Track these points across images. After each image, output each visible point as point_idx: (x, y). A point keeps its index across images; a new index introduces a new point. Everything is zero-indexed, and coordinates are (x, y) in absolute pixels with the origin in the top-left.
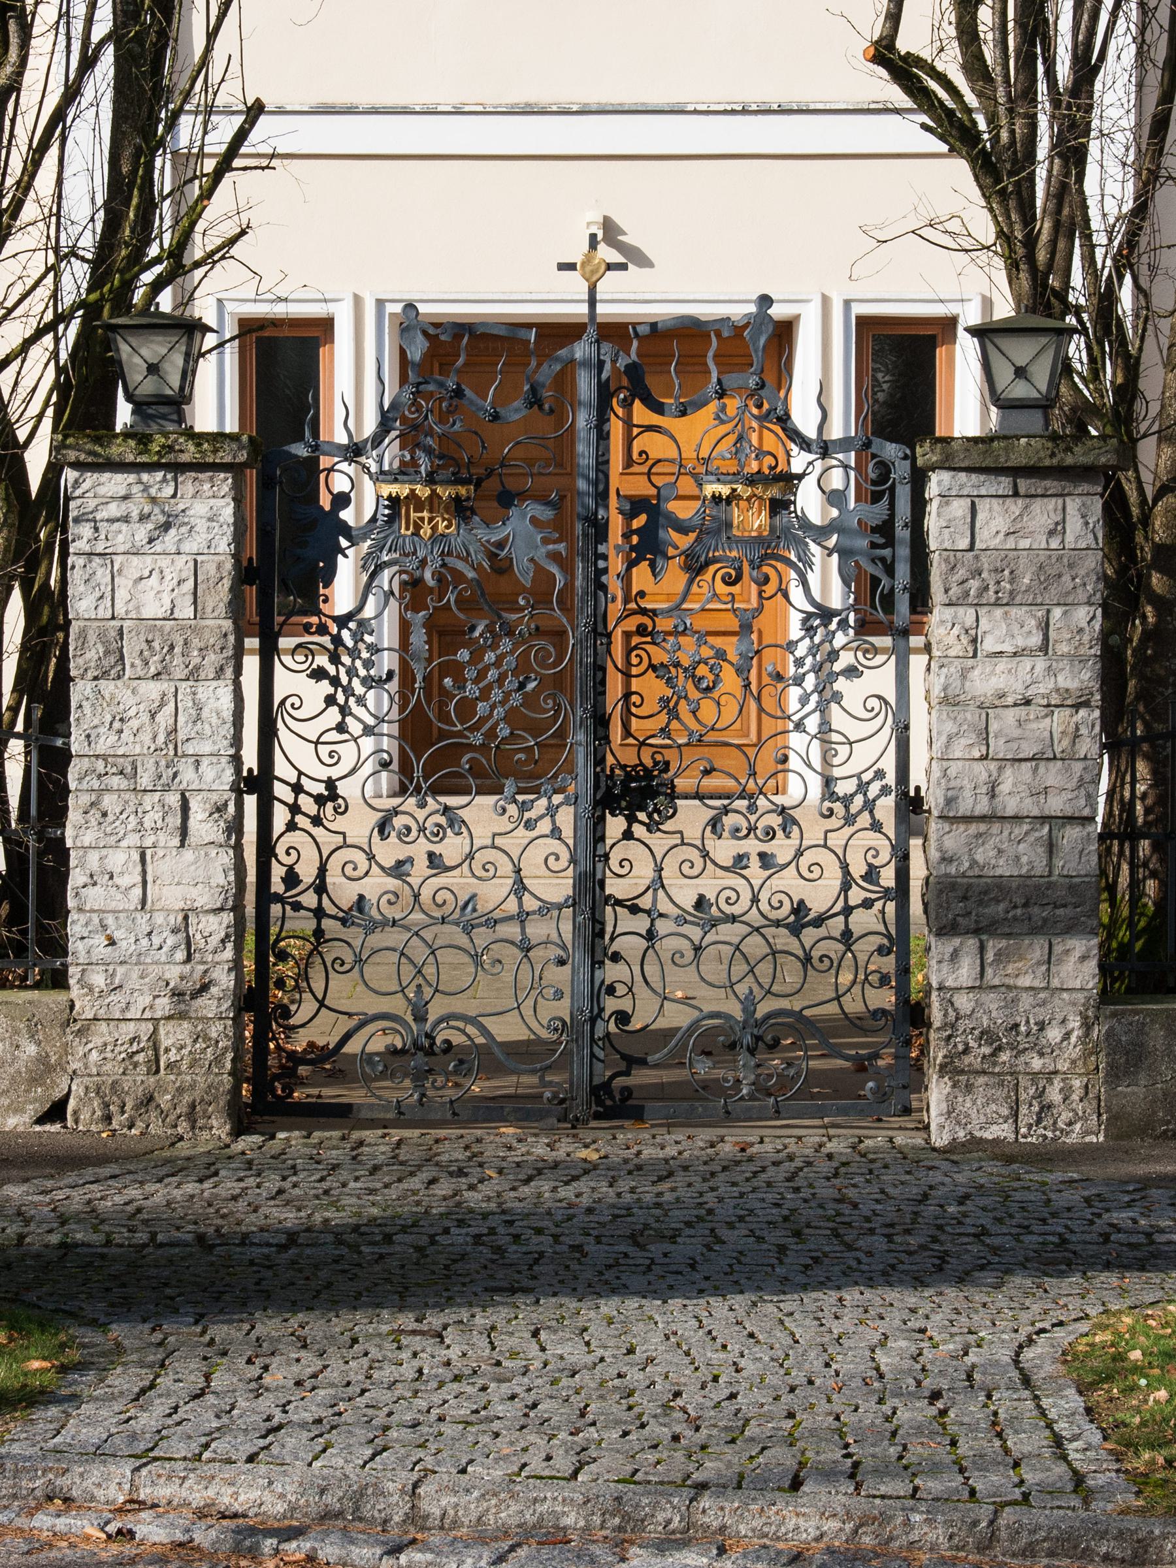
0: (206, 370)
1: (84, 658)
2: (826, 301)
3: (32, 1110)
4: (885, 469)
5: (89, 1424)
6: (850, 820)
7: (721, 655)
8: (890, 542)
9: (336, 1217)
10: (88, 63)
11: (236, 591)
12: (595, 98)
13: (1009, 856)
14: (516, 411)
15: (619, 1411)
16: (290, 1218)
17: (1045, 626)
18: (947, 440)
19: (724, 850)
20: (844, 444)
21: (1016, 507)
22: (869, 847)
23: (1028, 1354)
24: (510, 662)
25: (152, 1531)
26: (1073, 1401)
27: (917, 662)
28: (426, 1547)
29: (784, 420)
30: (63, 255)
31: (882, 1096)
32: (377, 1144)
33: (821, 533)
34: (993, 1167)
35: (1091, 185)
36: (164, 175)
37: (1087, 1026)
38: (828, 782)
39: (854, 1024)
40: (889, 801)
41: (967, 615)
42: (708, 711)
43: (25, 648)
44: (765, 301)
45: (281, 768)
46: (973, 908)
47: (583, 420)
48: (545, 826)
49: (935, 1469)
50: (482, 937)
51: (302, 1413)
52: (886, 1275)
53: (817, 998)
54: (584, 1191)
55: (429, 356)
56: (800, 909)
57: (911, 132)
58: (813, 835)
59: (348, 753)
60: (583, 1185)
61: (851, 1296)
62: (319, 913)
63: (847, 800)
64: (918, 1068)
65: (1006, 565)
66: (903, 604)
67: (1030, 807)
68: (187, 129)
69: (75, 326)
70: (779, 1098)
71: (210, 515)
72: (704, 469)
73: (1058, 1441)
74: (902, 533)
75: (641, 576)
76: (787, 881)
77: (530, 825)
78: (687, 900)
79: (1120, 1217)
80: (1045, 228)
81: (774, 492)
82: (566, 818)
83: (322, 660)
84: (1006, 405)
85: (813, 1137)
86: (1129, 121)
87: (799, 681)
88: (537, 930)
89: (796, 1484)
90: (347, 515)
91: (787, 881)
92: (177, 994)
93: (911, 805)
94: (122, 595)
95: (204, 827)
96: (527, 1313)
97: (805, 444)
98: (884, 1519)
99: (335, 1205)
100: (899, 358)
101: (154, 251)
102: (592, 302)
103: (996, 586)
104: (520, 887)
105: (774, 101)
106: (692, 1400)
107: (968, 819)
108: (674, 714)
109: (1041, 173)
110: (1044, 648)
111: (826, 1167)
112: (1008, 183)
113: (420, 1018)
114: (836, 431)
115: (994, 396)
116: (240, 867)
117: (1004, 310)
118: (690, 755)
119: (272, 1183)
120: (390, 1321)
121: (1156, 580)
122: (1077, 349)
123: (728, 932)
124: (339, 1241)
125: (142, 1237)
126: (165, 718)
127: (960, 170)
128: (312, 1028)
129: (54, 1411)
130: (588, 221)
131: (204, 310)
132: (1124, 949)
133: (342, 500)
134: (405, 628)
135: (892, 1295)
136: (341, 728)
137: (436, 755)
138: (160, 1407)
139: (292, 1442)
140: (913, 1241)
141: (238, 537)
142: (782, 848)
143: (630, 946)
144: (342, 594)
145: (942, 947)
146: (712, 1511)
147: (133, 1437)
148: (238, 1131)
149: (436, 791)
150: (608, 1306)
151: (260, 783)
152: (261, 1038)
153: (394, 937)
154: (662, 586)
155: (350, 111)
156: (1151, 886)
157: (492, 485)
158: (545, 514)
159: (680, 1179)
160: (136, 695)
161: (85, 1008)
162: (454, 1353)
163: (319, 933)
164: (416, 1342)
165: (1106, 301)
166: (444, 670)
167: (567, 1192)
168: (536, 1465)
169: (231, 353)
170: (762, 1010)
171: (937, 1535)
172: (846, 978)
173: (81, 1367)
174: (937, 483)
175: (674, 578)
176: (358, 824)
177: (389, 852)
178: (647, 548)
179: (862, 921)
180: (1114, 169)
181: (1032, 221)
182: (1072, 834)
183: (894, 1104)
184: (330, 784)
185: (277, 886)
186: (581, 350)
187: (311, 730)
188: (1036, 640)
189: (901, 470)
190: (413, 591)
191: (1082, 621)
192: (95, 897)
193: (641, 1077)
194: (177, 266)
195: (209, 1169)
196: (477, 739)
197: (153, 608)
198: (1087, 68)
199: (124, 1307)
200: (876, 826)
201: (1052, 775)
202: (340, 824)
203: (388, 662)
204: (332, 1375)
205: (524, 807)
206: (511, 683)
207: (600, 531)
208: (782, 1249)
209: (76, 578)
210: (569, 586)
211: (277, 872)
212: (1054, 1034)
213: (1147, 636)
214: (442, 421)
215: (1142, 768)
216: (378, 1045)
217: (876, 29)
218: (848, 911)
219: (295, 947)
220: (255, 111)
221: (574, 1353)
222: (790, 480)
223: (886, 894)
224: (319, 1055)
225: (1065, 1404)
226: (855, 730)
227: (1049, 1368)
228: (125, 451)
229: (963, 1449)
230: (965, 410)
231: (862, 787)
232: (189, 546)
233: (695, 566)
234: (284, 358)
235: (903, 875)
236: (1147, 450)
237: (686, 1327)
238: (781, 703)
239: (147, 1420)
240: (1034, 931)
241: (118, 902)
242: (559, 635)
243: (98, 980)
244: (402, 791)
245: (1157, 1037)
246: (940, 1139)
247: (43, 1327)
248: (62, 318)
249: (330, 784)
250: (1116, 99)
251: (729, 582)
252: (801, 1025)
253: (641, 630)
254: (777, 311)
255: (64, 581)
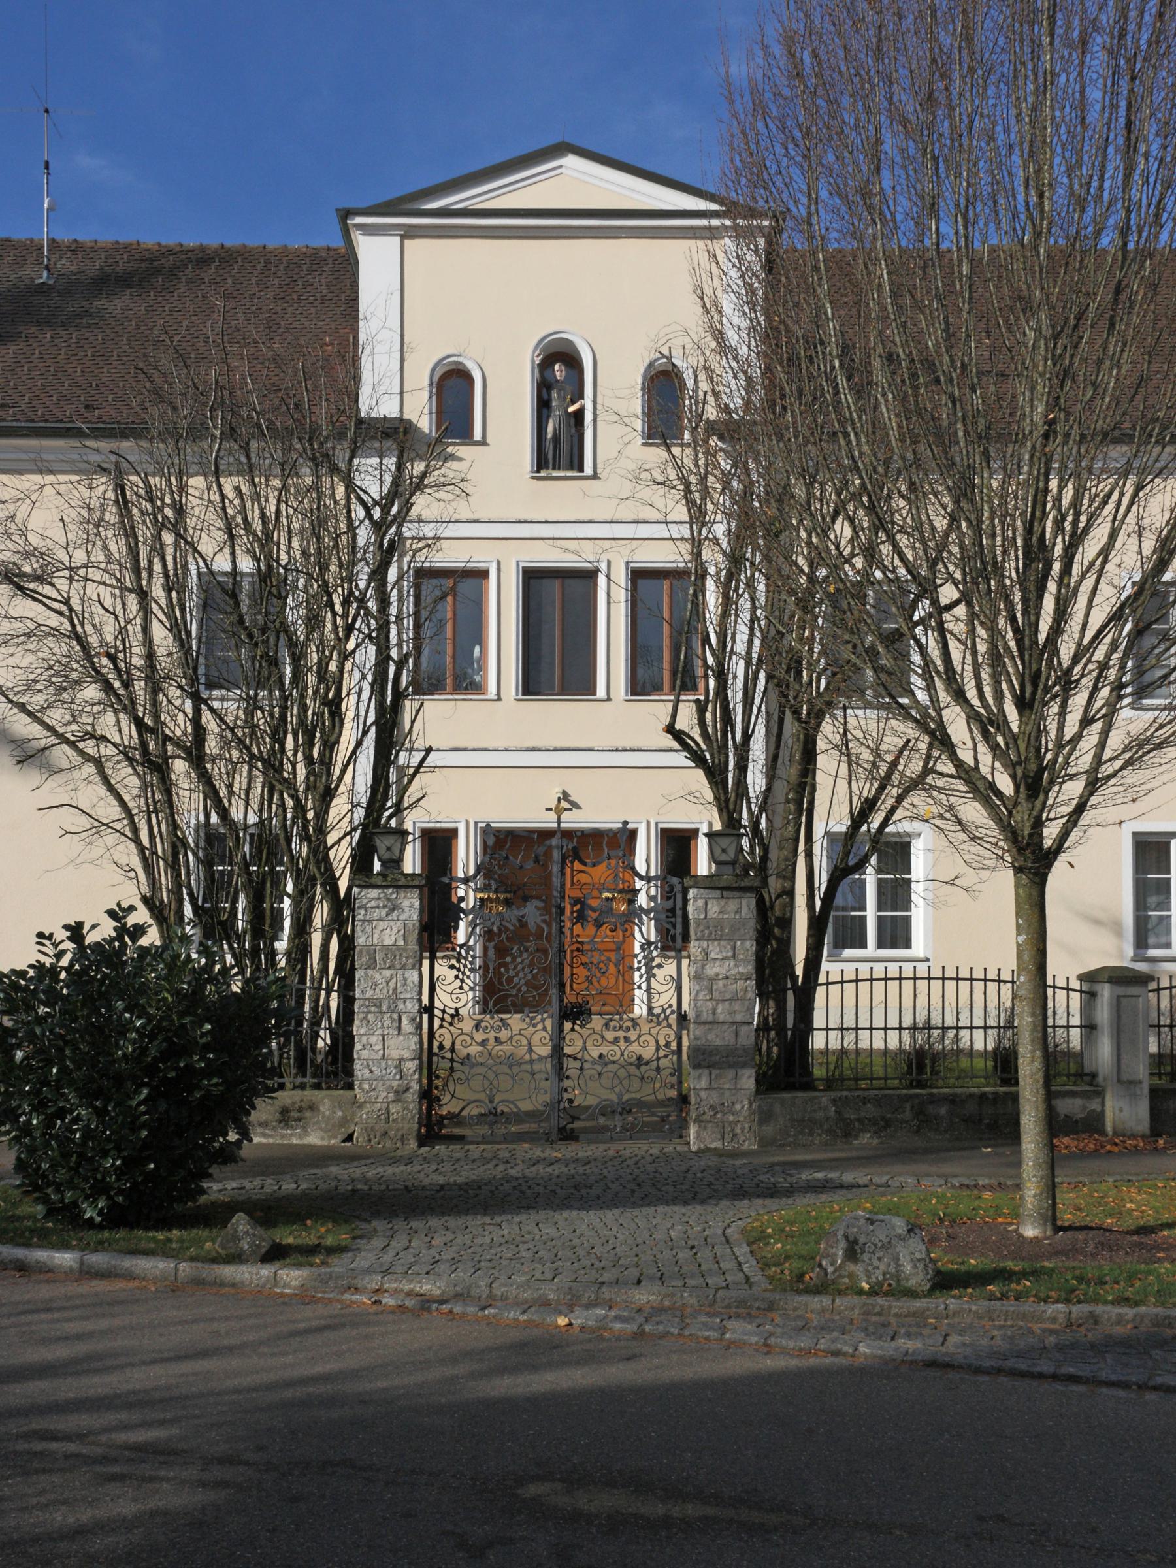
0: (409, 849)
1: (361, 960)
2: (648, 823)
3: (340, 1137)
4: (672, 888)
5: (364, 1260)
6: (659, 1024)
7: (609, 959)
8: (674, 916)
9: (459, 1180)
10: (365, 732)
11: (420, 934)
12: (559, 745)
13: (719, 1038)
14: (530, 865)
15: (569, 1254)
16: (441, 1180)
17: (734, 948)
18: (696, 876)
19: (610, 1036)
20: (656, 878)
21: (722, 902)
22: (666, 1034)
23: (728, 1231)
24: (527, 962)
25: (389, 1301)
26: (745, 1249)
27: (685, 962)
28: (495, 1307)
29: (633, 868)
30: (355, 805)
31: (671, 1131)
32: (475, 1150)
33: (647, 912)
34: (715, 1159)
35: (749, 780)
36: (393, 775)
37: (751, 1104)
38: (650, 1009)
39: (661, 1103)
40: (674, 1016)
41: (705, 944)
42: (604, 981)
43: (338, 957)
44: (625, 823)
45: (437, 1004)
46: (704, 1058)
47: (555, 869)
48: (540, 1026)
49: (692, 1276)
50: (515, 1070)
51: (447, 1256)
52: (674, 1201)
53: (646, 1093)
54: (556, 1170)
55: (496, 843)
56: (640, 1058)
57: (681, 759)
58: (645, 1030)
59: (463, 997)
60: (555, 1166)
61: (660, 1209)
62: (452, 1060)
63: (658, 1016)
64: (685, 1120)
65: (719, 923)
66: (679, 939)
67: (729, 1019)
68: (403, 758)
69: (358, 833)
70: (632, 1132)
71: (411, 905)
72: (602, 887)
73: (740, 1264)
74: (679, 913)
75: (578, 929)
76: (635, 1047)
77: (535, 1026)
78: (595, 1054)
79: (762, 1178)
80: (732, 796)
81: (629, 896)
82: (549, 1023)
83: (454, 962)
84: (718, 863)
85: (645, 1147)
86: (763, 756)
87: (639, 969)
88: (536, 1067)
89: (639, 1282)
90: (463, 905)
91: (635, 1047)
92: (397, 1092)
93: (682, 1018)
94: (376, 936)
95: (406, 1026)
96: (534, 1216)
97: (641, 878)
98: (672, 1295)
99: (458, 1174)
100: (677, 844)
101: (389, 804)
102: (559, 822)
103: (715, 931)
104: (530, 1050)
105: (628, 745)
106: (598, 1250)
107: (705, 1023)
108: (590, 982)
109: (731, 775)
110: (734, 956)
111: (649, 1159)
112: (718, 778)
113: (491, 1101)
114: (653, 874)
115: (713, 857)
116: (421, 1042)
117: (718, 826)
118: (597, 998)
119: (434, 1167)
120: (480, 1220)
121: (776, 931)
122: (745, 843)
123: (610, 1067)
124: (460, 1189)
125: (383, 1187)
126: (392, 984)
127: (700, 773)
128: (448, 1105)
129: (350, 1254)
130: (556, 793)
131: (408, 826)
132: (765, 1073)
133: (462, 899)
134: (485, 949)
135: (676, 1208)
136: (461, 988)
137: (496, 997)
138: (391, 1253)
139: (442, 1267)
140: (684, 1187)
141: (421, 913)
142: (633, 1034)
143: (574, 1073)
144: (461, 936)
145: (694, 1073)
146: (606, 1293)
147: (382, 1264)
148: (421, 1145)
149: (498, 1012)
150: (566, 1214)
151: (429, 1009)
152: (429, 1109)
153: (482, 1070)
154: (585, 932)
155: (465, 750)
156: (775, 1049)
157: (520, 893)
158: (542, 904)
159: (593, 1164)
160: (381, 976)
161: (361, 1097)
162: (505, 1232)
163: (452, 1068)
164: (491, 1228)
165: (755, 824)
166: (500, 965)
167: (549, 1170)
168: (538, 1275)
169: (418, 843)
170: (625, 1098)
171: (693, 1301)
172: (657, 1085)
173: (361, 1237)
174: (692, 893)
175: (591, 929)
176: (467, 1026)
177: (479, 1037)
178: (581, 917)
179: (664, 1063)
180: (759, 774)
181: (728, 799)
182: (744, 1030)
183: (676, 1134)
184: (457, 1010)
185: (436, 1050)
186: (555, 842)
187: (449, 989)
188: (730, 954)
189: (678, 888)
190: (488, 935)
191: (750, 946)
192: (365, 1054)
193: (577, 1124)
194: (398, 809)
195: (409, 1161)
196: (514, 992)
197: (388, 941)
198: (747, 737)
199: (376, 1214)
200: (669, 1026)
201: (737, 1006)
202: (460, 1025)
203: (478, 962)
204: (459, 1241)
205: (532, 1019)
206: (527, 970)
207: (562, 911)
208: (633, 1191)
209: (358, 929)
210: (550, 933)
211: (436, 1044)
212: (738, 1107)
213: (773, 952)
214: (500, 867)
215: (771, 1003)
216: (475, 1112)
217: (667, 720)
218: (658, 1059)
219: (442, 1073)
220: (429, 750)
221: (552, 1232)
222: (635, 892)
223: (673, 1052)
224: (452, 1116)
225: (742, 1250)
226: (661, 988)
227: (737, 1236)
228: (374, 880)
229: (703, 1267)
230: (703, 865)
231: (664, 1011)
232: (403, 917)
233: (599, 925)
234: (438, 843)
235: (679, 1045)
236: (772, 881)
237: (596, 1222)
238: (632, 978)
239: (387, 1258)
240: (730, 1066)
241: (374, 1056)
242: (545, 952)
243: (366, 1086)
244: (484, 1012)
245: (777, 1108)
246: (694, 1148)
247: (346, 1221)
248: (354, 829)
249: (457, 1010)
250: (758, 747)
251: (612, 931)
252: (641, 1104)
253: (578, 950)
254: (630, 826)
255: (353, 931)
